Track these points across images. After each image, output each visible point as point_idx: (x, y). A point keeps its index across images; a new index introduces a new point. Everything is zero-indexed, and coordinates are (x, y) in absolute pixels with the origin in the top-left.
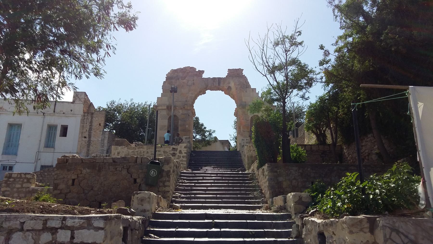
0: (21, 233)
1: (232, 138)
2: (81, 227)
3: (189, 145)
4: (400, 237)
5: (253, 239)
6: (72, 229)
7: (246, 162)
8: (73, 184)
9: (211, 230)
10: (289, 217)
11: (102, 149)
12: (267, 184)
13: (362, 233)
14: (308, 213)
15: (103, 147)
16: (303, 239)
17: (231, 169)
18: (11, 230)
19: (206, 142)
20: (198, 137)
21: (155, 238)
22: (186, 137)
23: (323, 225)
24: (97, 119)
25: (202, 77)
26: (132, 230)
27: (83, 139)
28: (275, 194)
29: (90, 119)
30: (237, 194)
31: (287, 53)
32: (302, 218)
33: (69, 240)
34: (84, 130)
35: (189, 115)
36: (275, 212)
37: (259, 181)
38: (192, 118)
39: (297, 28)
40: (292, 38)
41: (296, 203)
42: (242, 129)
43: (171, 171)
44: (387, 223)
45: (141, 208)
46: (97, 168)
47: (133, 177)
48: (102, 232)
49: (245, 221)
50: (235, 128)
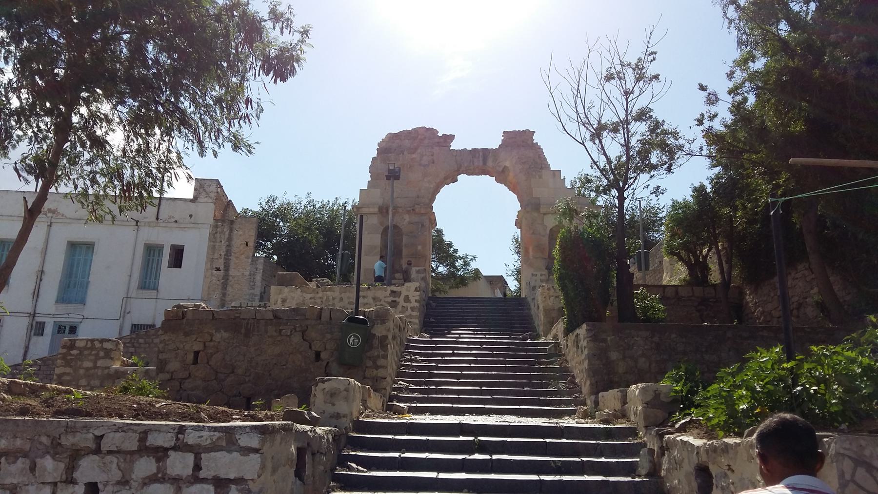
0: (96, 458)
2: (214, 448)
3: (423, 285)
5: (558, 478)
6: (197, 451)
8: (195, 362)
9: (472, 457)
10: (632, 432)
11: (251, 291)
12: (586, 365)
14: (673, 425)
15: (254, 289)
16: (662, 478)
19: (458, 280)
20: (442, 269)
21: (359, 471)
22: (418, 268)
23: (707, 451)
24: (241, 233)
26: (313, 454)
27: (214, 272)
29: (227, 233)
30: (522, 385)
32: (661, 436)
34: (216, 256)
35: (423, 225)
37: (569, 358)
38: (430, 231)
39: (650, 45)
41: (648, 405)
43: (390, 337)
44: (845, 449)
45: (330, 410)
46: (243, 331)
47: (313, 348)
48: (255, 458)
49: (542, 440)
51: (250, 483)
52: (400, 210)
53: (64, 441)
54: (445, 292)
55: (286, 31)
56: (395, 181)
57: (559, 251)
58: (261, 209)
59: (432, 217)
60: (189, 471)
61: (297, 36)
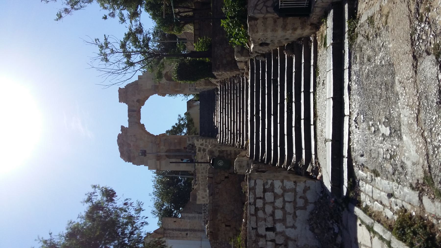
0: (258, 229)
1: (186, 98)
2: (255, 193)
3: (195, 138)
4: (260, 4)
6: (256, 198)
7: (209, 87)
8: (229, 226)
10: (252, 60)
11: (197, 218)
12: (229, 73)
13: (258, 25)
14: (249, 49)
15: (196, 217)
17: (216, 100)
18: (256, 235)
20: (185, 131)
21: (265, 156)
22: (188, 141)
25: (128, 127)
26: (259, 169)
27: (188, 236)
28: (237, 68)
29: (170, 231)
31: (115, 52)
32: (252, 53)
33: (262, 200)
34: (181, 235)
35: (166, 140)
36: (249, 70)
37: (226, 78)
38: (168, 136)
40: (101, 47)
41: (242, 55)
42: (178, 89)
43: (219, 149)
44: (251, 12)
47: (223, 179)
48: (257, 181)
49: (255, 92)
50: (176, 95)
51: (264, 182)
52: (158, 150)
53: (254, 239)
54: (196, 129)
55: (95, 194)
56: (147, 152)
57: (183, 81)
58: (158, 217)
59: (162, 135)
60: (261, 200)
61: (97, 189)
